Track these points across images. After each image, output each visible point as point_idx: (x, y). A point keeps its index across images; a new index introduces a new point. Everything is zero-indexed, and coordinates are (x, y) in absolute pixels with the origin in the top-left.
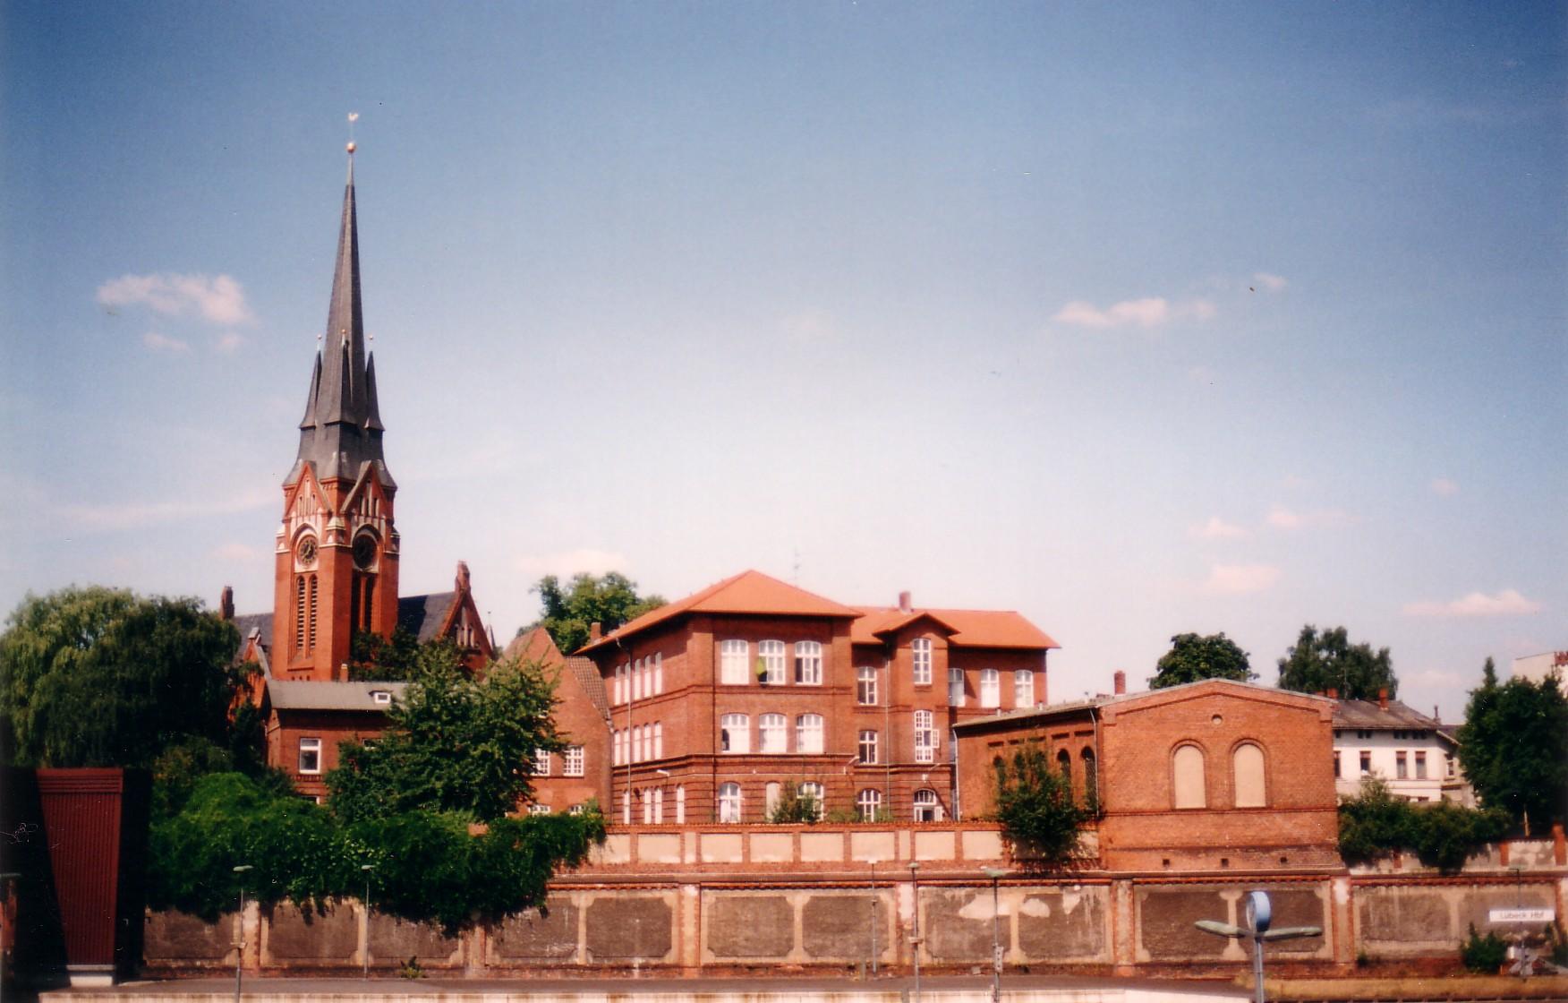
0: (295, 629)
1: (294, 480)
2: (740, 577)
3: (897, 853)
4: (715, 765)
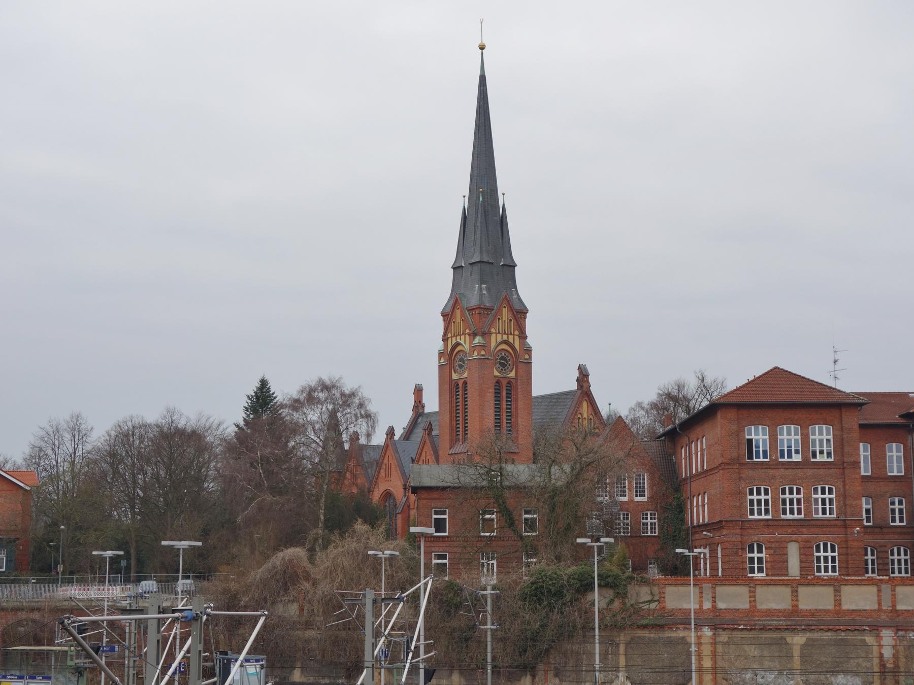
0: (454, 423)
1: (449, 310)
2: (772, 370)
3: (880, 603)
4: (845, 526)
